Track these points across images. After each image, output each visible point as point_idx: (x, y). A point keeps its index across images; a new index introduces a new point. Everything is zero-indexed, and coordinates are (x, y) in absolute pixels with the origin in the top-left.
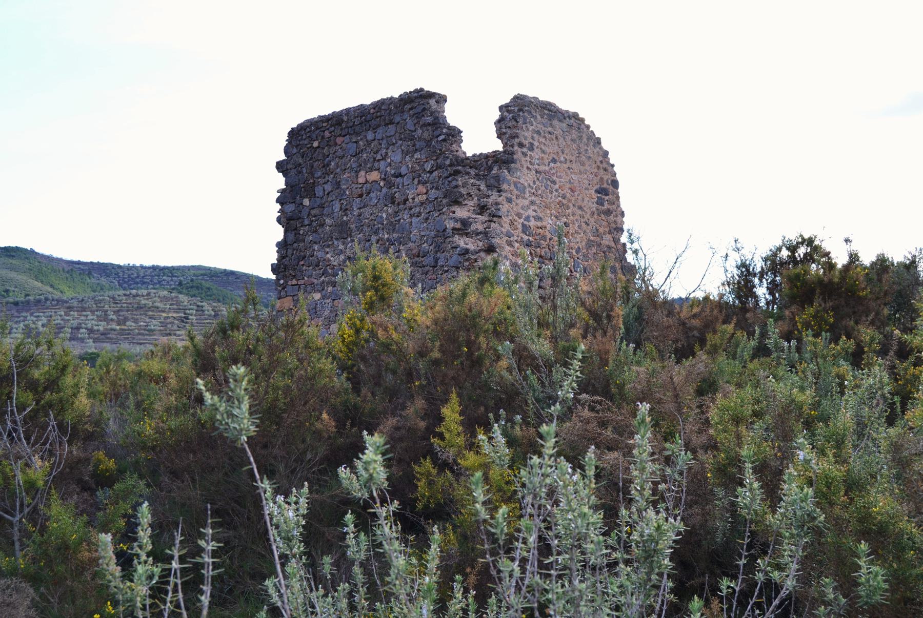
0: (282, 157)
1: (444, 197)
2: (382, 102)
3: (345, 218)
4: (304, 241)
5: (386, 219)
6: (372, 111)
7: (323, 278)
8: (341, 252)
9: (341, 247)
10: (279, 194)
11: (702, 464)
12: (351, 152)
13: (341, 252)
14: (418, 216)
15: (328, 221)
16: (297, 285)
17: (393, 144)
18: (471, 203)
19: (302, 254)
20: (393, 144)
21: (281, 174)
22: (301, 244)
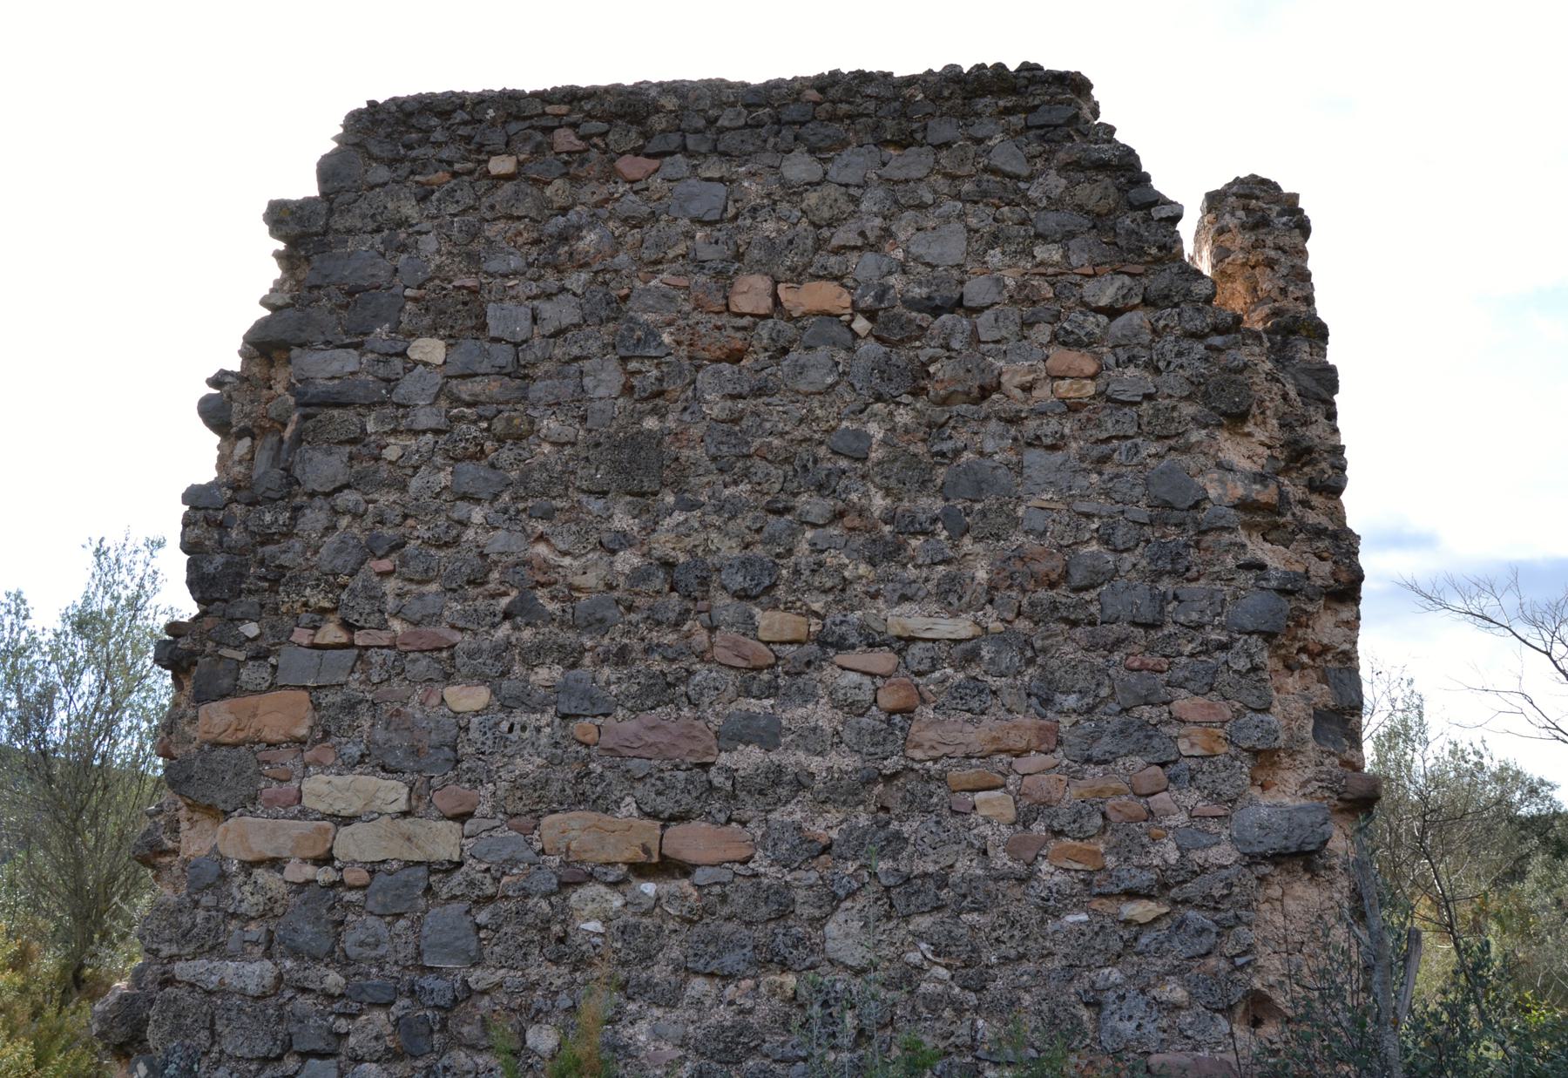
0: (309, 188)
1: (1188, 398)
2: (862, 77)
3: (651, 423)
4: (403, 487)
5: (884, 442)
6: (812, 95)
7: (505, 628)
8: (624, 540)
9: (622, 520)
10: (267, 313)
11: (477, 1064)
12: (696, 209)
13: (624, 540)
14: (1053, 448)
15: (550, 424)
16: (350, 645)
17: (921, 206)
18: (1261, 435)
19: (388, 532)
20: (921, 206)
21: (789, 78)
22: (385, 498)
